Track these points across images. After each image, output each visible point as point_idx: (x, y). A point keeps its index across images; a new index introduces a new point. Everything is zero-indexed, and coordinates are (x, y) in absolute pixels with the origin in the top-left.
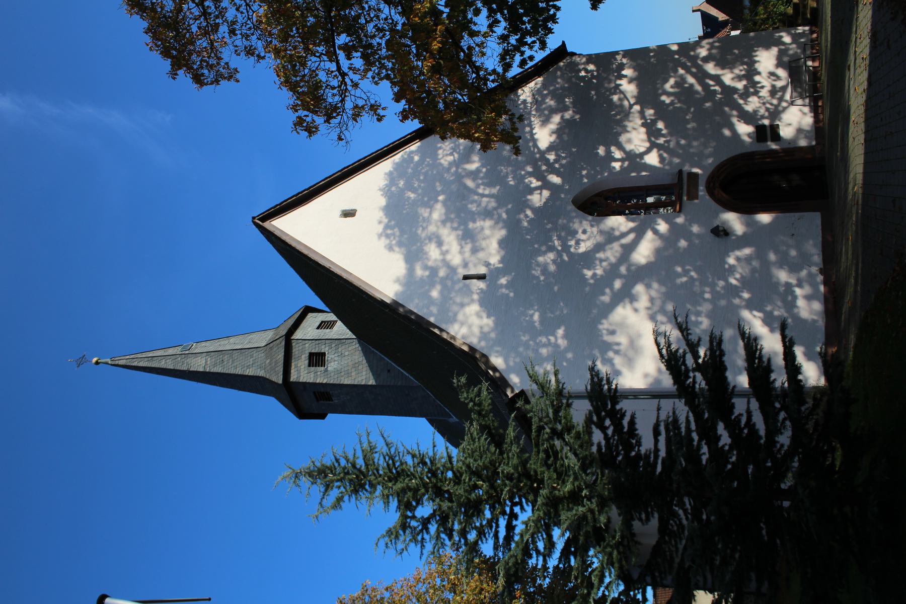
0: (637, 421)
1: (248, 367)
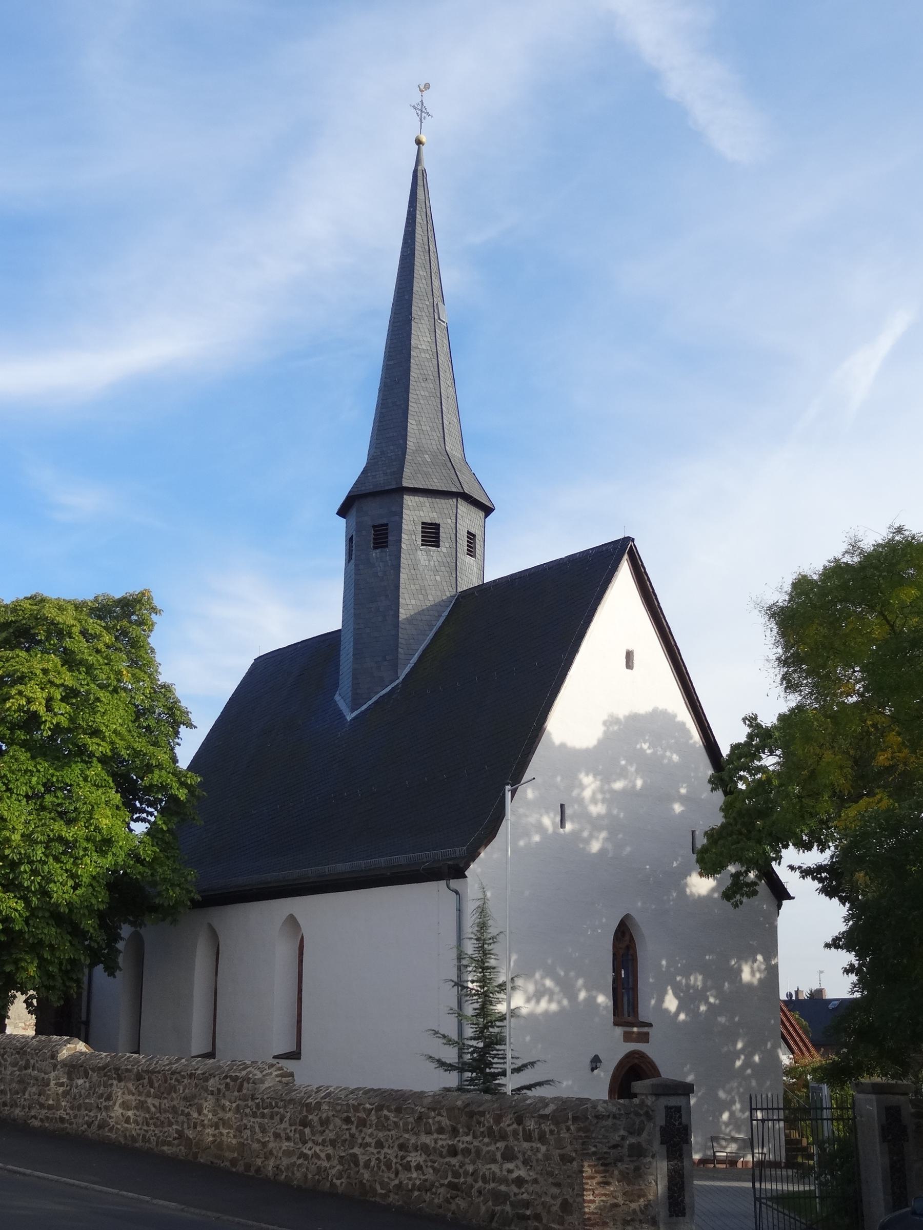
1: (419, 423)
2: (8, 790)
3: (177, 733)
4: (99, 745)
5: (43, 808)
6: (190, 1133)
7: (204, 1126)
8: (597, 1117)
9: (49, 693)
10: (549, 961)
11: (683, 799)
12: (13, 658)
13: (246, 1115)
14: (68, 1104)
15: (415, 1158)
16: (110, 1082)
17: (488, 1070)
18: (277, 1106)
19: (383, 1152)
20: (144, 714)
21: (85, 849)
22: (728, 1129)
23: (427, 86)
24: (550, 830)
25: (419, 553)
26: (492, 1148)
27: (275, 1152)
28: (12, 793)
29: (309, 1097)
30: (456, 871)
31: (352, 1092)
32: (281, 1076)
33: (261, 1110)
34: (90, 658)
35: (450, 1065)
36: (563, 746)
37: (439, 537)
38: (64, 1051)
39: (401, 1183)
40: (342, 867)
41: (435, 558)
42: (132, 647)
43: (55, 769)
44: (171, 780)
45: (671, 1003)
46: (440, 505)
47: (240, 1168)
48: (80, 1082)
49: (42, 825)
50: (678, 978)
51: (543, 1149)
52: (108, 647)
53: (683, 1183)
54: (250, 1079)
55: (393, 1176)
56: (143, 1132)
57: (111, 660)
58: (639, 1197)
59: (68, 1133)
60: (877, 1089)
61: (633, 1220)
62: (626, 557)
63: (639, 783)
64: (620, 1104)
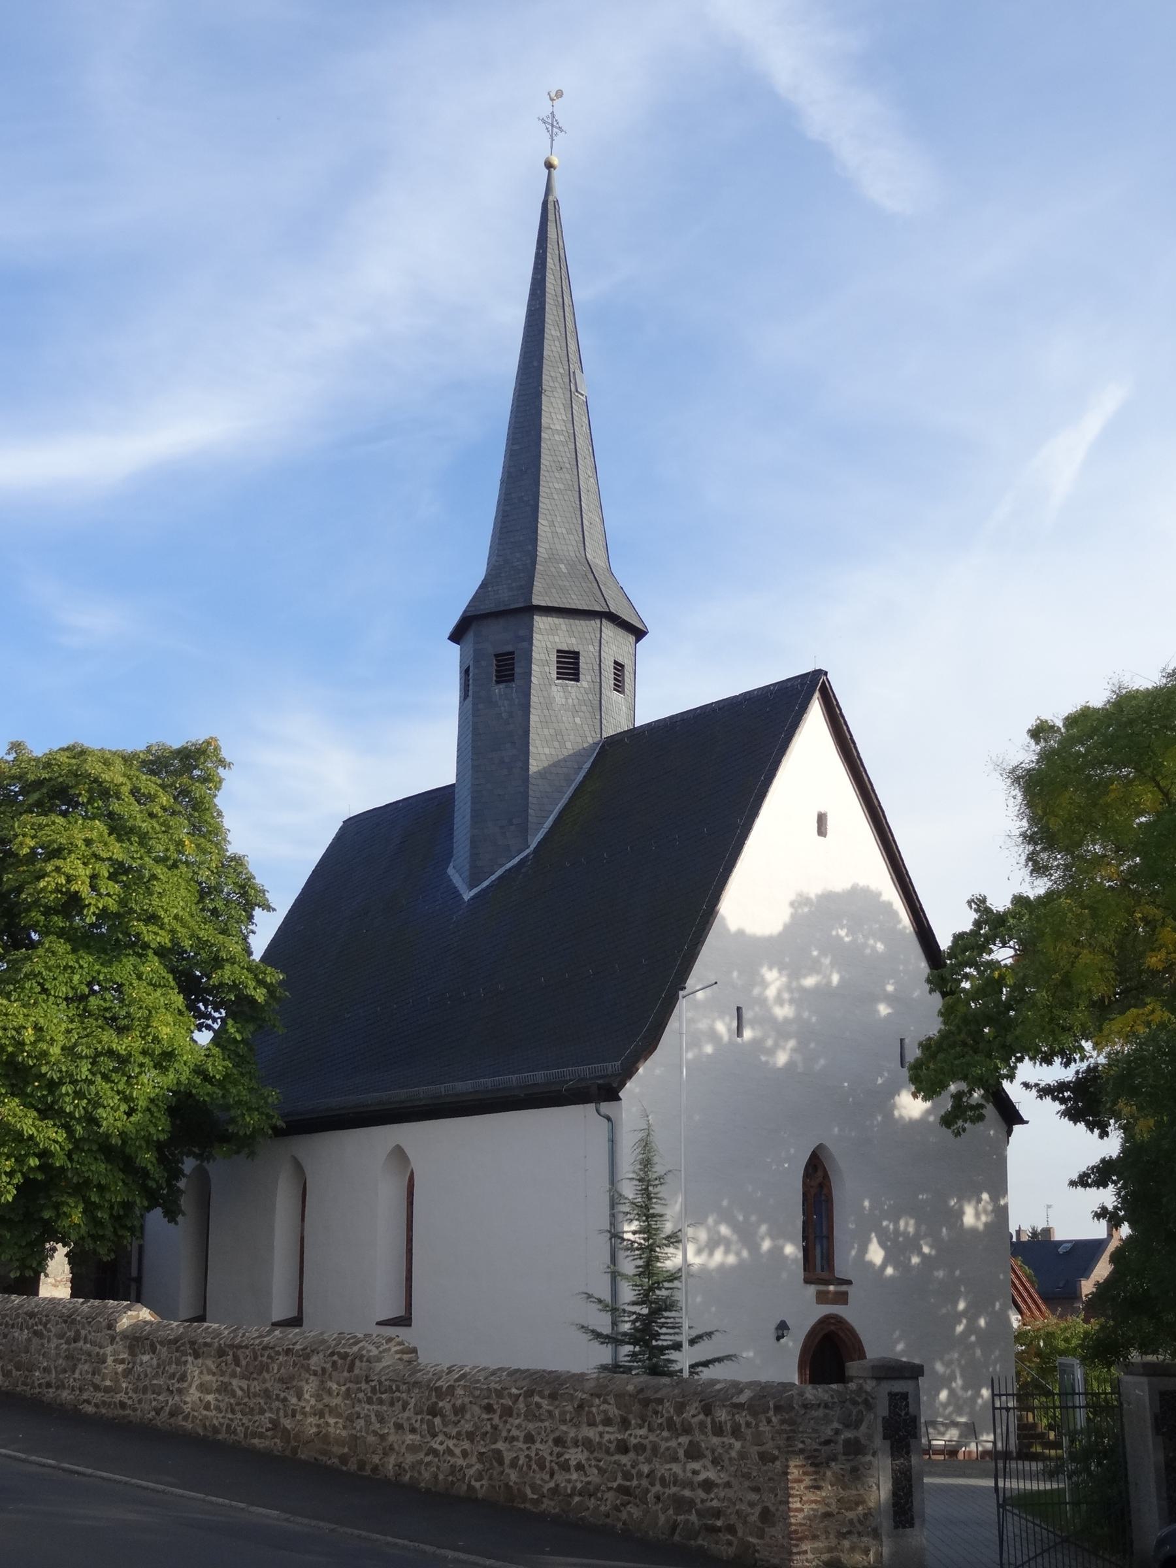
0: (65, 746)
1: (552, 524)
2: (45, 991)
3: (250, 918)
4: (156, 934)
5: (86, 1013)
6: (287, 1423)
7: (304, 1414)
8: (805, 1406)
9: (94, 869)
10: (725, 1203)
11: (889, 999)
12: (47, 825)
13: (359, 1401)
14: (130, 1386)
15: (575, 1455)
16: (184, 1359)
17: (654, 1343)
18: (398, 1390)
19: (534, 1447)
20: (210, 893)
21: (141, 1065)
22: (960, 1414)
23: (559, 94)
24: (726, 1038)
25: (554, 688)
26: (673, 1444)
27: (396, 1446)
28: (48, 995)
29: (439, 1379)
30: (608, 1092)
31: (493, 1373)
32: (402, 1352)
33: (379, 1395)
34: (144, 825)
35: (607, 1337)
36: (741, 933)
37: (578, 669)
38: (124, 1320)
39: (557, 1485)
40: (462, 1087)
41: (573, 695)
42: (194, 809)
43: (102, 964)
44: (246, 978)
45: (876, 1254)
46: (580, 629)
47: (353, 1466)
48: (146, 1358)
49: (87, 1036)
50: (885, 1223)
51: (738, 1445)
52: (164, 809)
53: (911, 1486)
54: (362, 1356)
55: (547, 1477)
56: (227, 1421)
57: (170, 827)
58: (857, 1504)
59: (131, 1422)
60: (1150, 1370)
61: (849, 1532)
62: (817, 695)
63: (835, 979)
64: (833, 1390)
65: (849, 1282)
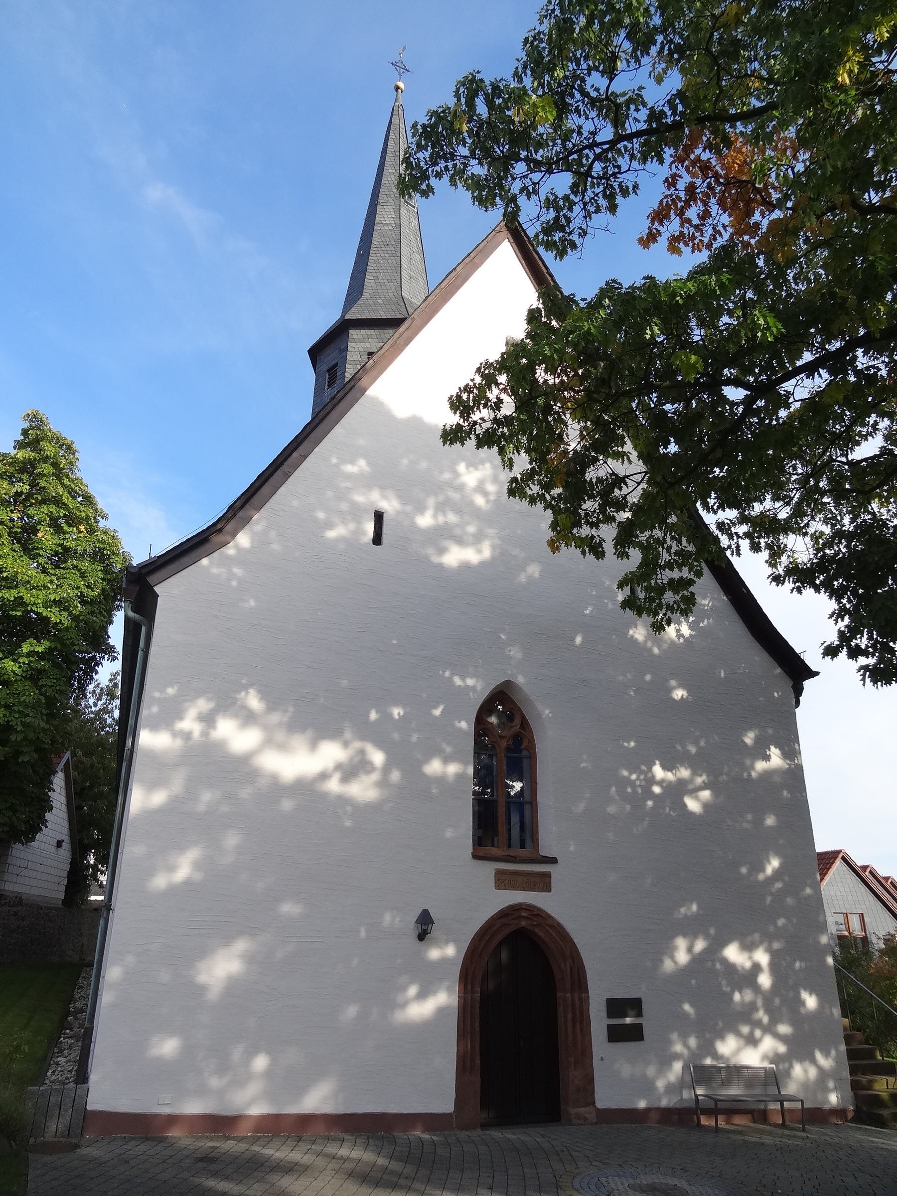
65: (553, 861)
